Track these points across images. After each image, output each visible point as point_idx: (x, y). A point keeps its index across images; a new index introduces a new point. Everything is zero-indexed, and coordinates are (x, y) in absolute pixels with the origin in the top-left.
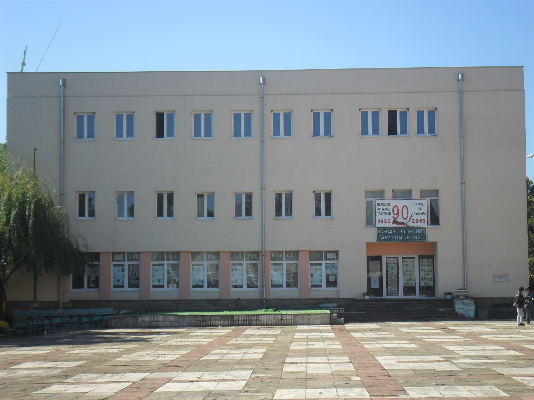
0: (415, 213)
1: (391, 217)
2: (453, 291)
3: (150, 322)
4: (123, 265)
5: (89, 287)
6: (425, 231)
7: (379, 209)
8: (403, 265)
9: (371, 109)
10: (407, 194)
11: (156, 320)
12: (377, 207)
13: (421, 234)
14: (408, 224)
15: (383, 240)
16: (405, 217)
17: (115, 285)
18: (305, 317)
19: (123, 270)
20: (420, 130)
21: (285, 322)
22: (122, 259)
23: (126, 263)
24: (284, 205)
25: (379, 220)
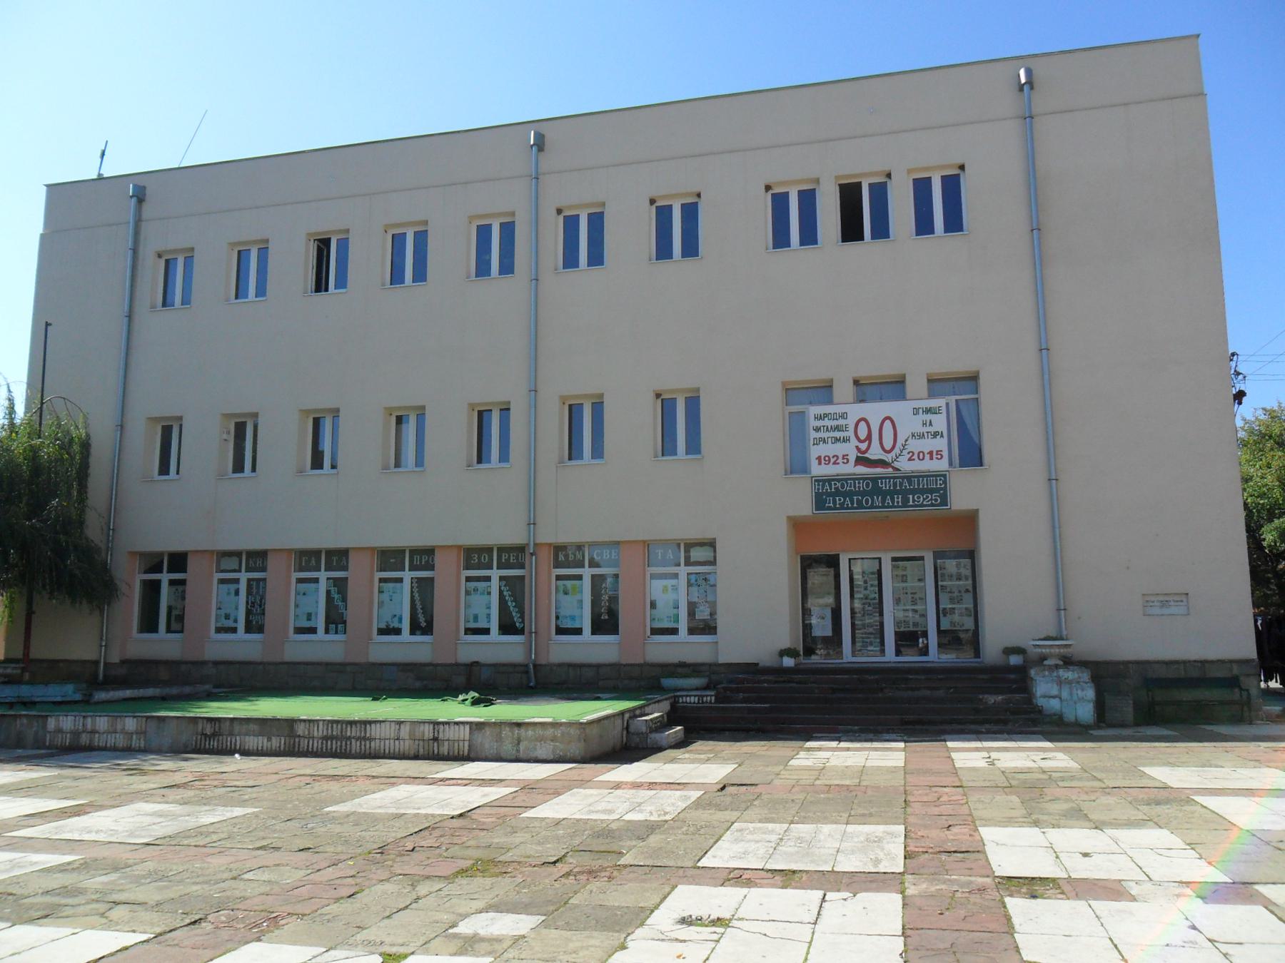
0: (914, 435)
1: (850, 449)
2: (1028, 643)
3: (76, 734)
4: (237, 581)
6: (945, 482)
7: (817, 429)
8: (894, 577)
10: (894, 387)
11: (89, 727)
12: (814, 423)
13: (931, 491)
14: (896, 464)
15: (829, 508)
16: (888, 447)
17: (219, 625)
19: (237, 593)
20: (924, 225)
21: (444, 750)
23: (244, 577)
24: (583, 425)
25: (819, 458)
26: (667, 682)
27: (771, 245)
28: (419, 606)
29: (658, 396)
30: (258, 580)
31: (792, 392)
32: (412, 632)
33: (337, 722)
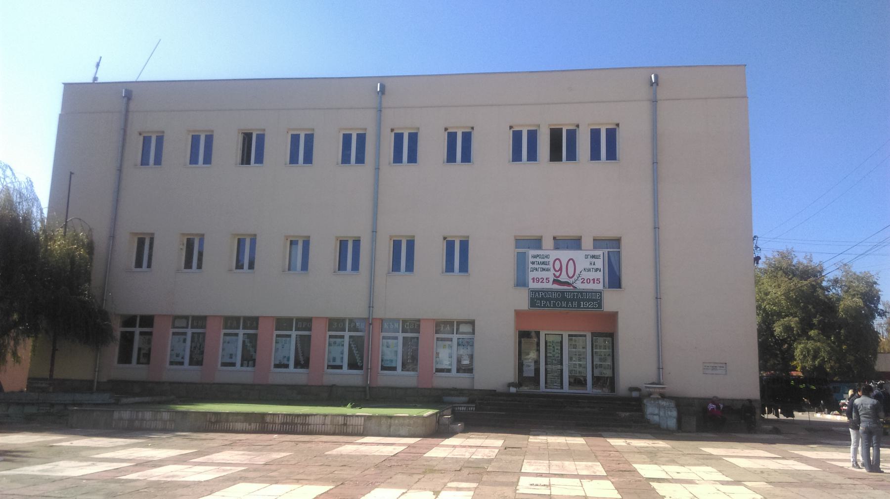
0: (585, 270)
1: (550, 275)
4: (185, 334)
5: (138, 363)
7: (533, 263)
8: (570, 345)
9: (527, 125)
10: (575, 243)
12: (531, 260)
13: (594, 300)
16: (571, 275)
18: (383, 421)
19: (185, 341)
20: (595, 155)
21: (350, 430)
22: (185, 325)
23: (189, 332)
25: (533, 279)
26: (447, 399)
27: (340, 161)
28: (299, 350)
29: (445, 238)
30: (199, 334)
31: (521, 242)
32: (295, 367)
33: (290, 415)
